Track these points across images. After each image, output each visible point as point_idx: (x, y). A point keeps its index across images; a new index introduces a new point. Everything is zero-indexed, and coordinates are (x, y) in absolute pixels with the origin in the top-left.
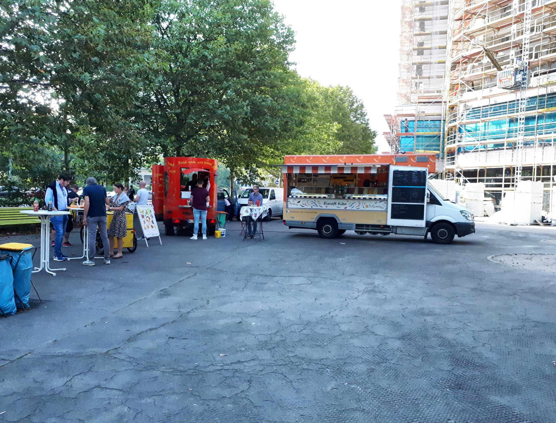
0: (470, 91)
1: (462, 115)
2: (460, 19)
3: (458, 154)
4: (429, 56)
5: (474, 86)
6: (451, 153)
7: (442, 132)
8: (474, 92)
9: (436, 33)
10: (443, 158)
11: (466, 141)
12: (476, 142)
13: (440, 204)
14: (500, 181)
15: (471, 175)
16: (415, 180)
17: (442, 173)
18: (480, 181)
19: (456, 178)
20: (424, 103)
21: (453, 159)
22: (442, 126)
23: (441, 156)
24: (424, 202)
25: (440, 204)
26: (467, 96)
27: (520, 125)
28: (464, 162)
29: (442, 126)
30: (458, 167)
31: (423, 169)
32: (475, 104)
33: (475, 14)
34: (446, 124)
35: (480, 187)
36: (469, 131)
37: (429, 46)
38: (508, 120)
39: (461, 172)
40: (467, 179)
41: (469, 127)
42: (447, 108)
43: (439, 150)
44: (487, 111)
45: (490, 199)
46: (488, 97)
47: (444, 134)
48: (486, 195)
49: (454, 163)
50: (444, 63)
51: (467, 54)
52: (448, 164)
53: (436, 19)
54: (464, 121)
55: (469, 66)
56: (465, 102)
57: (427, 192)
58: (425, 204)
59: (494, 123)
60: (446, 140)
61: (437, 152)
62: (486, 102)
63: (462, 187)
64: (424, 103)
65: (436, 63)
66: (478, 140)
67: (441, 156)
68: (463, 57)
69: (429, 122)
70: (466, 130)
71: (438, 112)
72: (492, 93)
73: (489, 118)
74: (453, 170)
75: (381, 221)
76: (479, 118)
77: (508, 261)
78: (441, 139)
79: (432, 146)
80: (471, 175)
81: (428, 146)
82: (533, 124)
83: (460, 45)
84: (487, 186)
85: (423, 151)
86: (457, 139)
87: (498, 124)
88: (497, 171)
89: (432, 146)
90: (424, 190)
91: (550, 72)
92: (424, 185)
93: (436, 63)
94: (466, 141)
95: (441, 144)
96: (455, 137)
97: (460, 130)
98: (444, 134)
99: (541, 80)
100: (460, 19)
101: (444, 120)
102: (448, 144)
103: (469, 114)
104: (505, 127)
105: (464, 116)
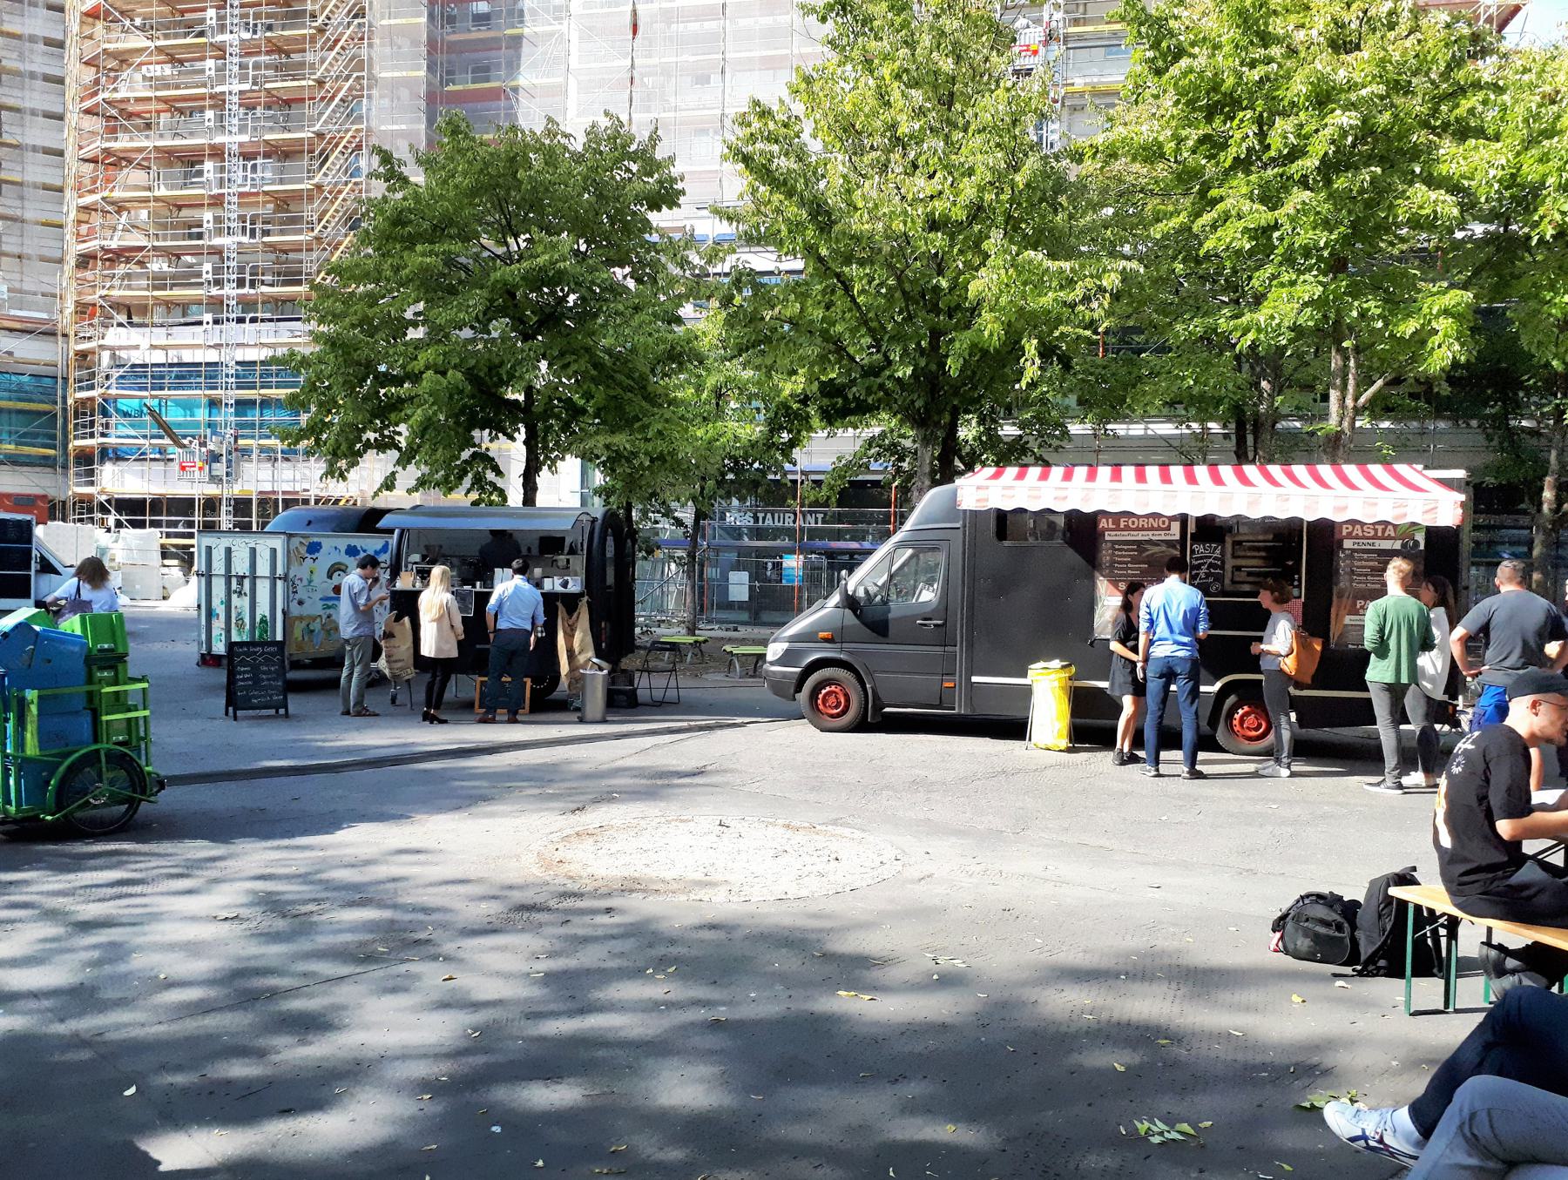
0: (120, 325)
1: (107, 377)
2: (94, 161)
3: (102, 462)
4: (18, 203)
5: (133, 313)
6: (86, 460)
7: (59, 406)
8: (133, 330)
9: (35, 149)
10: (65, 467)
11: (119, 434)
12: (142, 441)
13: (57, 573)
14: (190, 524)
15: (134, 511)
16: (12, 535)
17: (64, 503)
18: (154, 524)
19: (98, 515)
20: (11, 330)
21: (91, 473)
22: (60, 392)
23: (60, 460)
24: (29, 568)
25: (57, 573)
26: (116, 336)
27: (227, 416)
28: (116, 481)
29: (60, 392)
30: (102, 492)
31: (28, 517)
32: (136, 357)
33: (130, 161)
34: (70, 390)
35: (152, 537)
36: (126, 414)
37: (16, 178)
38: (204, 401)
39: (108, 501)
40: (122, 518)
41: (123, 405)
42: (71, 354)
43: (54, 447)
44: (162, 377)
45: (175, 562)
46: (164, 348)
47: (65, 410)
48: (164, 555)
49: (92, 483)
50: (61, 226)
51: (114, 244)
52: (78, 485)
53: (33, 113)
54: (113, 391)
55: (121, 269)
56: (112, 349)
57: (34, 552)
58: (33, 573)
59: (178, 403)
60: (71, 426)
61: (51, 452)
62: (158, 357)
63: (113, 535)
64: (11, 330)
65: (37, 223)
66: (145, 437)
67: (60, 460)
68: (102, 248)
69: (25, 379)
70: (117, 410)
71: (48, 357)
72: (171, 342)
73: (166, 392)
74: (90, 498)
75: (1147, 505)
76: (146, 389)
77: (157, 647)
78: (60, 422)
79: (36, 435)
80: (134, 511)
81: (25, 435)
82: (254, 416)
83: (97, 219)
84: (168, 535)
85: (12, 447)
86: (98, 429)
87: (188, 406)
88: (183, 506)
89: (36, 435)
90: (30, 550)
91: (279, 320)
92: (30, 542)
93: (37, 223)
94: (119, 434)
95: (59, 434)
96: (92, 424)
97: (105, 413)
98: (65, 410)
99: (264, 333)
100: (94, 161)
101: (65, 379)
102: (76, 437)
103: (122, 377)
104: (202, 415)
105: (113, 380)
